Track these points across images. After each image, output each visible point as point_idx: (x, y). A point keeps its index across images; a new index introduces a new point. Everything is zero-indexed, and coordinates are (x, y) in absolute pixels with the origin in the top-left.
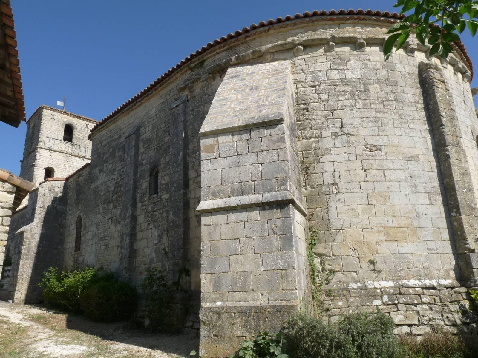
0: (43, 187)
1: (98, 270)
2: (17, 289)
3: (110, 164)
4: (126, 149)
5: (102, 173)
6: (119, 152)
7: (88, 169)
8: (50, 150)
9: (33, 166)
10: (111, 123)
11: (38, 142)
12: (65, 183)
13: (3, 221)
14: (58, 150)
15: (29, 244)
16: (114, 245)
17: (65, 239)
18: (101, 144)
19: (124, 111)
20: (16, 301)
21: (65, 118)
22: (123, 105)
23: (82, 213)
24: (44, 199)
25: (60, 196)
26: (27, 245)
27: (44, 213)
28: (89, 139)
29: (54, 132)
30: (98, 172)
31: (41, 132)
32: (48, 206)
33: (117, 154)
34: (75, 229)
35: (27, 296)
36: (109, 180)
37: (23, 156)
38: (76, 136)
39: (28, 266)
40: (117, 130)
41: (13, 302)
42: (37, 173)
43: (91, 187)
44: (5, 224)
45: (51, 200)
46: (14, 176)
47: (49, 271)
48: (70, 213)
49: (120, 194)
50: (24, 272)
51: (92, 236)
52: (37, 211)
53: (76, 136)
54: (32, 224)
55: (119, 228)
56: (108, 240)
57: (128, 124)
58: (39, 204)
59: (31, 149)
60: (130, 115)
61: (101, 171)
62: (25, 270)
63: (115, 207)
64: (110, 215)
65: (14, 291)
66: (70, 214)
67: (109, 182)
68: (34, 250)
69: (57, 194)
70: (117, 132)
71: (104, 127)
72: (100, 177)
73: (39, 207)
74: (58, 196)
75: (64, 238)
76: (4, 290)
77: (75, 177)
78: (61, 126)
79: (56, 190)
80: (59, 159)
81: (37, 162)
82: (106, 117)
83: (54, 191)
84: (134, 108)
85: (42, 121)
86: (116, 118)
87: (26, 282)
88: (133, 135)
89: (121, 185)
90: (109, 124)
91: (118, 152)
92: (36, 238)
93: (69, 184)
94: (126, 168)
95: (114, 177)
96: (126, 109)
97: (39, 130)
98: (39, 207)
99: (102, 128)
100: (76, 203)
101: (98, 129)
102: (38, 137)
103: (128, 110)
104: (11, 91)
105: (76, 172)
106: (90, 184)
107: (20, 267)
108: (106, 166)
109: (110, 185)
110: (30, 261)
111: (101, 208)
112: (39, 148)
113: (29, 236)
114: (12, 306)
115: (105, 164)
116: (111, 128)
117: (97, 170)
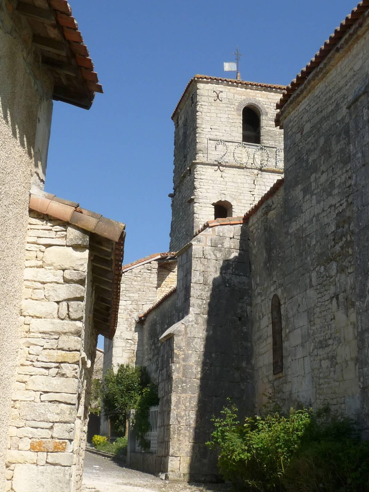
0: (199, 241)
1: (319, 415)
2: (171, 451)
3: (323, 172)
4: (352, 132)
5: (308, 197)
6: (338, 142)
7: (281, 192)
8: (219, 165)
9: (192, 201)
10: (317, 78)
11: (195, 153)
12: (242, 229)
13: (70, 309)
14: (234, 163)
15: (184, 360)
16: (348, 358)
17: (255, 348)
18: (301, 130)
19: (339, 46)
20: (171, 475)
21: (241, 94)
22: (336, 31)
23: (280, 290)
24: (204, 265)
25: (236, 257)
26: (181, 362)
27: (209, 294)
28: (276, 126)
29: (224, 128)
30: (301, 194)
31: (199, 130)
32: (215, 280)
33: (336, 148)
34: (271, 326)
35: (192, 466)
36: (323, 211)
37: (172, 185)
38: (267, 128)
39: (188, 404)
40: (331, 94)
41: (167, 478)
42: (200, 217)
43: (290, 231)
44: (74, 315)
45: (219, 267)
46: (83, 211)
47: (224, 417)
48: (258, 290)
49: (349, 239)
50: (182, 417)
51: (302, 338)
52: (193, 292)
53: (267, 128)
54: (186, 318)
55: (353, 317)
56: (335, 347)
57: (352, 73)
58: (196, 277)
59: (185, 168)
60: (354, 51)
61: (306, 190)
62: (183, 414)
63: (341, 270)
64: (332, 290)
65: (167, 455)
66: (259, 294)
67: (324, 214)
68: (194, 371)
69: (230, 253)
70: (331, 98)
71: (302, 92)
72: (305, 206)
73: (196, 283)
74: (232, 256)
75: (252, 345)
76: (151, 453)
77: (259, 213)
78: (235, 113)
79: (227, 244)
80: (239, 181)
81: (197, 192)
82: (304, 69)
83: (223, 246)
84: (359, 33)
85: (198, 108)
86: (325, 65)
87: (187, 438)
88: (363, 97)
89: (349, 218)
90: (312, 83)
91: (337, 143)
92: (198, 347)
93: (251, 229)
94: (354, 176)
95: (333, 202)
96: (343, 41)
97: (195, 128)
98: (196, 283)
99: (298, 95)
100: (268, 268)
101: (291, 98)
102: (194, 142)
103: (347, 42)
104: (54, 26)
105: (261, 202)
106: (287, 224)
107: (172, 407)
108: (316, 179)
109: (326, 220)
110: (189, 394)
111: (314, 275)
112: (198, 163)
113: (183, 344)
114: (165, 486)
115: (314, 175)
116: (316, 92)
117: (298, 192)
